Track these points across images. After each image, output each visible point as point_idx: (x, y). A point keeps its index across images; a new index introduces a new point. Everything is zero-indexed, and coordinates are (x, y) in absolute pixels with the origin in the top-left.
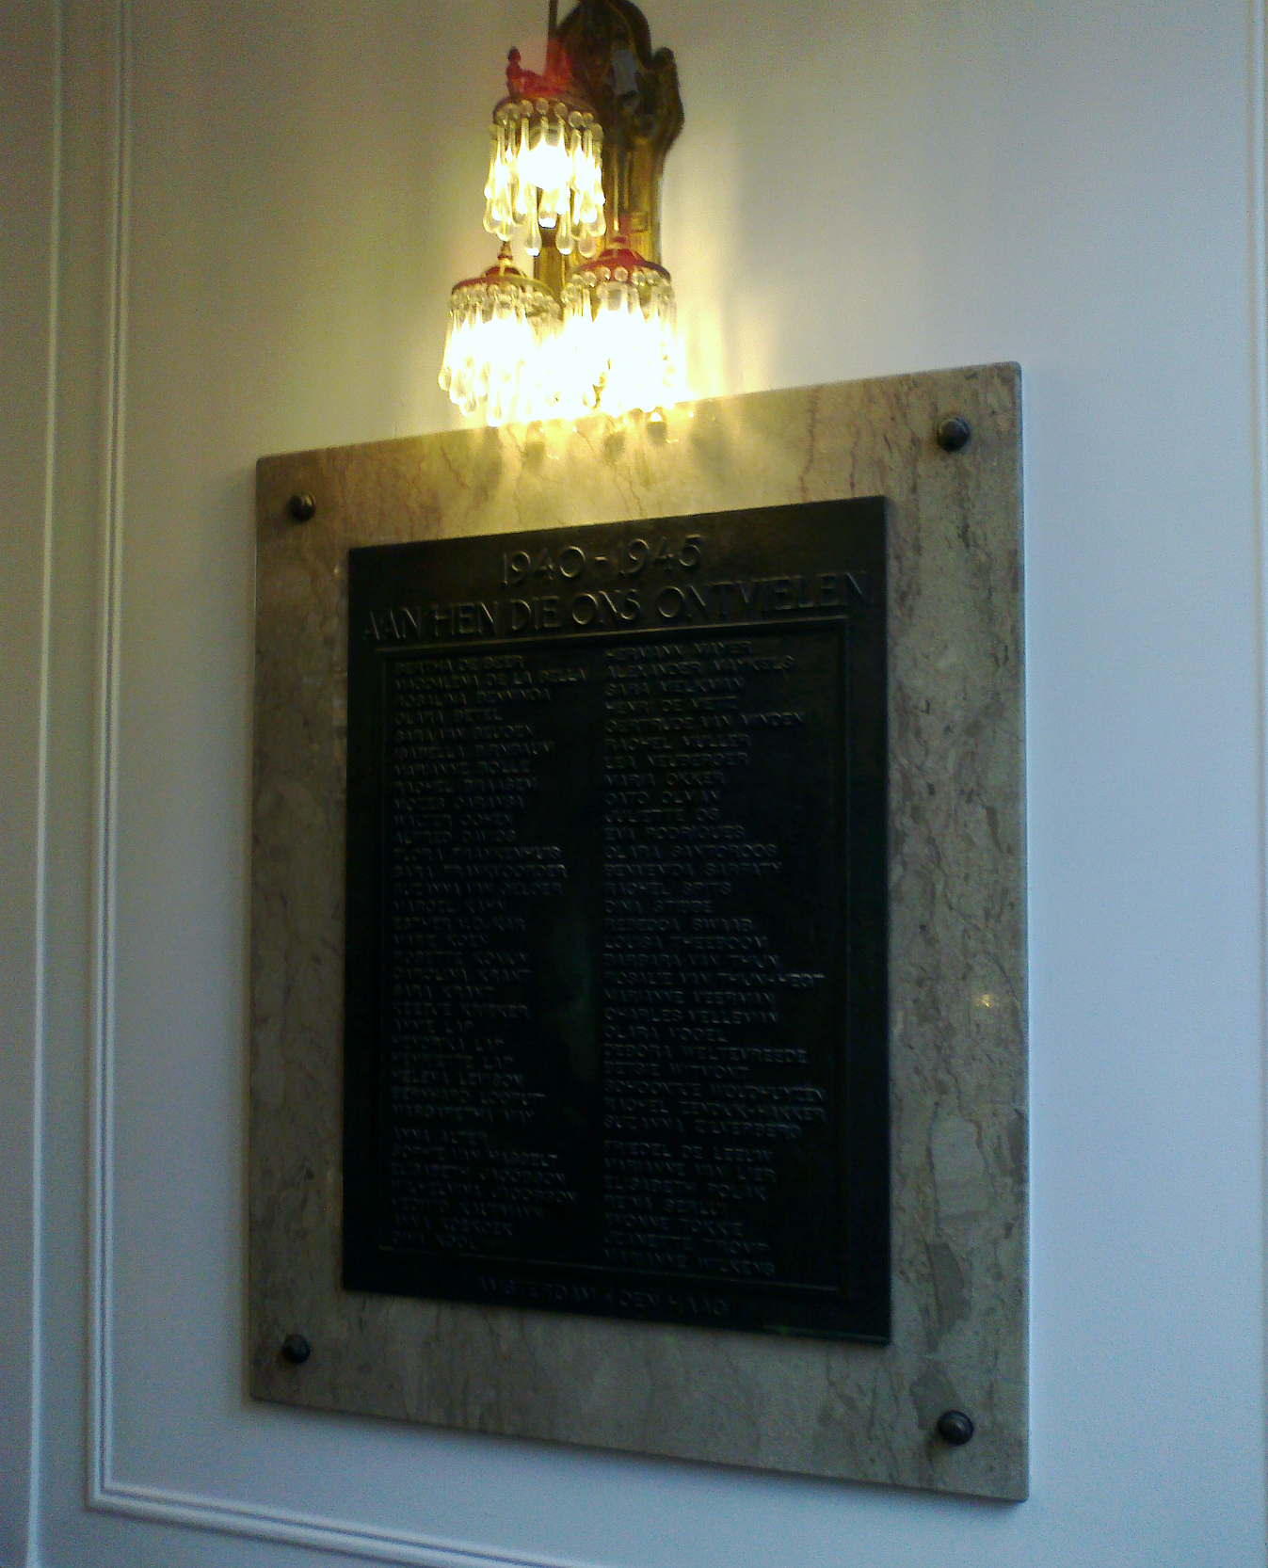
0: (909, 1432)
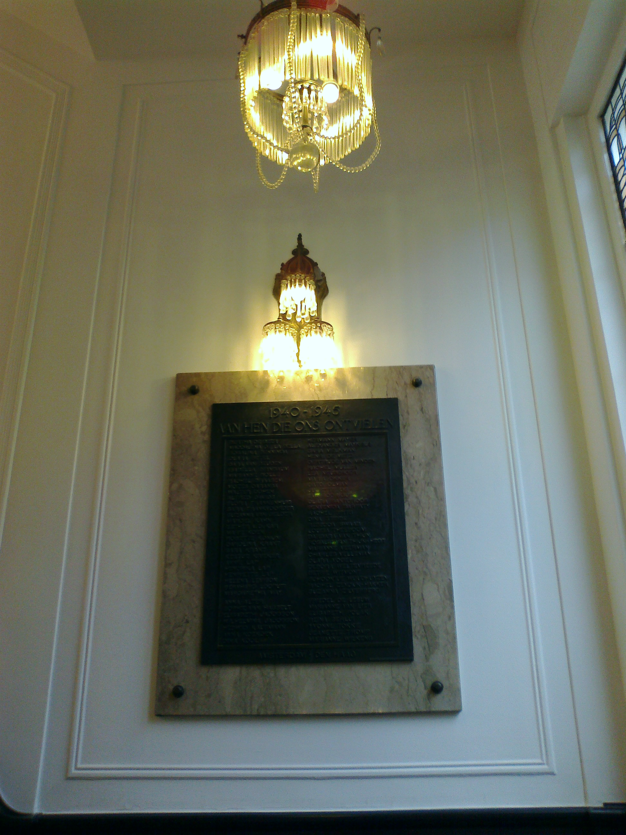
0: (421, 691)
